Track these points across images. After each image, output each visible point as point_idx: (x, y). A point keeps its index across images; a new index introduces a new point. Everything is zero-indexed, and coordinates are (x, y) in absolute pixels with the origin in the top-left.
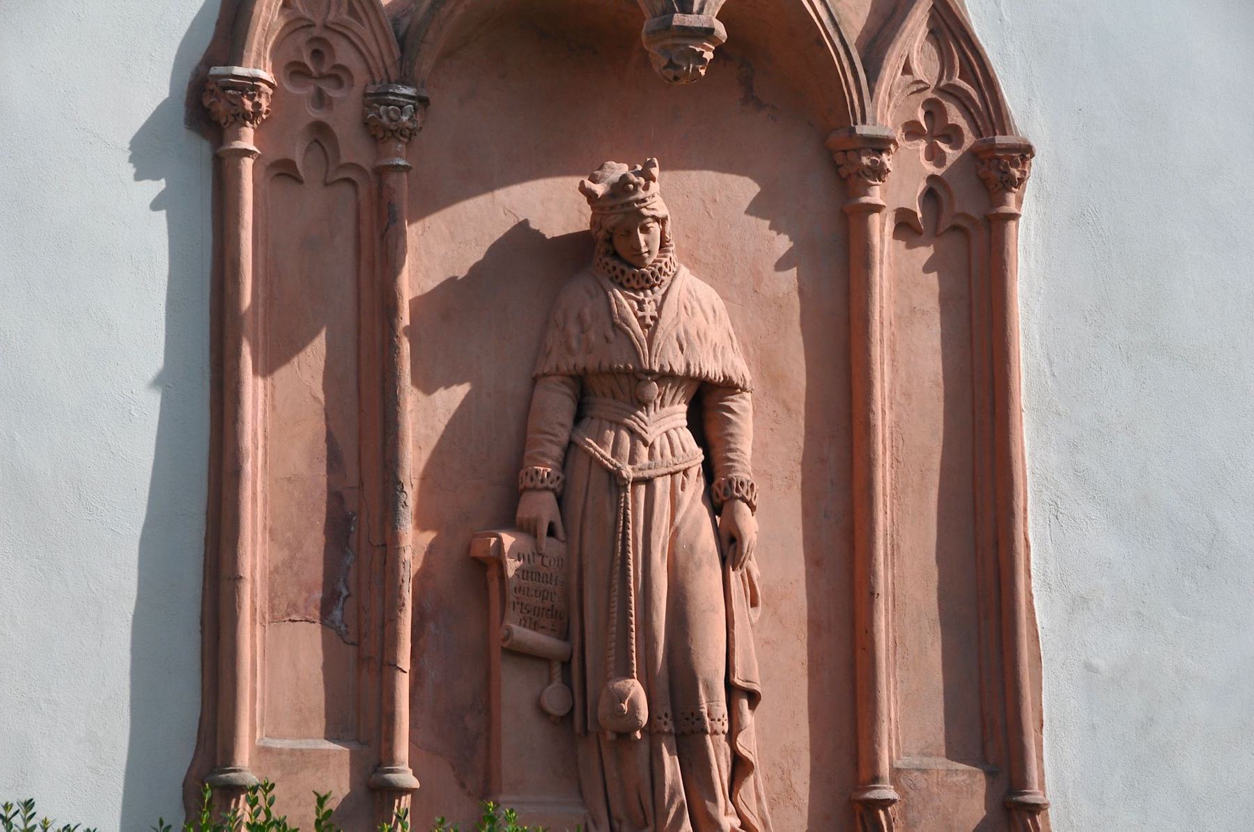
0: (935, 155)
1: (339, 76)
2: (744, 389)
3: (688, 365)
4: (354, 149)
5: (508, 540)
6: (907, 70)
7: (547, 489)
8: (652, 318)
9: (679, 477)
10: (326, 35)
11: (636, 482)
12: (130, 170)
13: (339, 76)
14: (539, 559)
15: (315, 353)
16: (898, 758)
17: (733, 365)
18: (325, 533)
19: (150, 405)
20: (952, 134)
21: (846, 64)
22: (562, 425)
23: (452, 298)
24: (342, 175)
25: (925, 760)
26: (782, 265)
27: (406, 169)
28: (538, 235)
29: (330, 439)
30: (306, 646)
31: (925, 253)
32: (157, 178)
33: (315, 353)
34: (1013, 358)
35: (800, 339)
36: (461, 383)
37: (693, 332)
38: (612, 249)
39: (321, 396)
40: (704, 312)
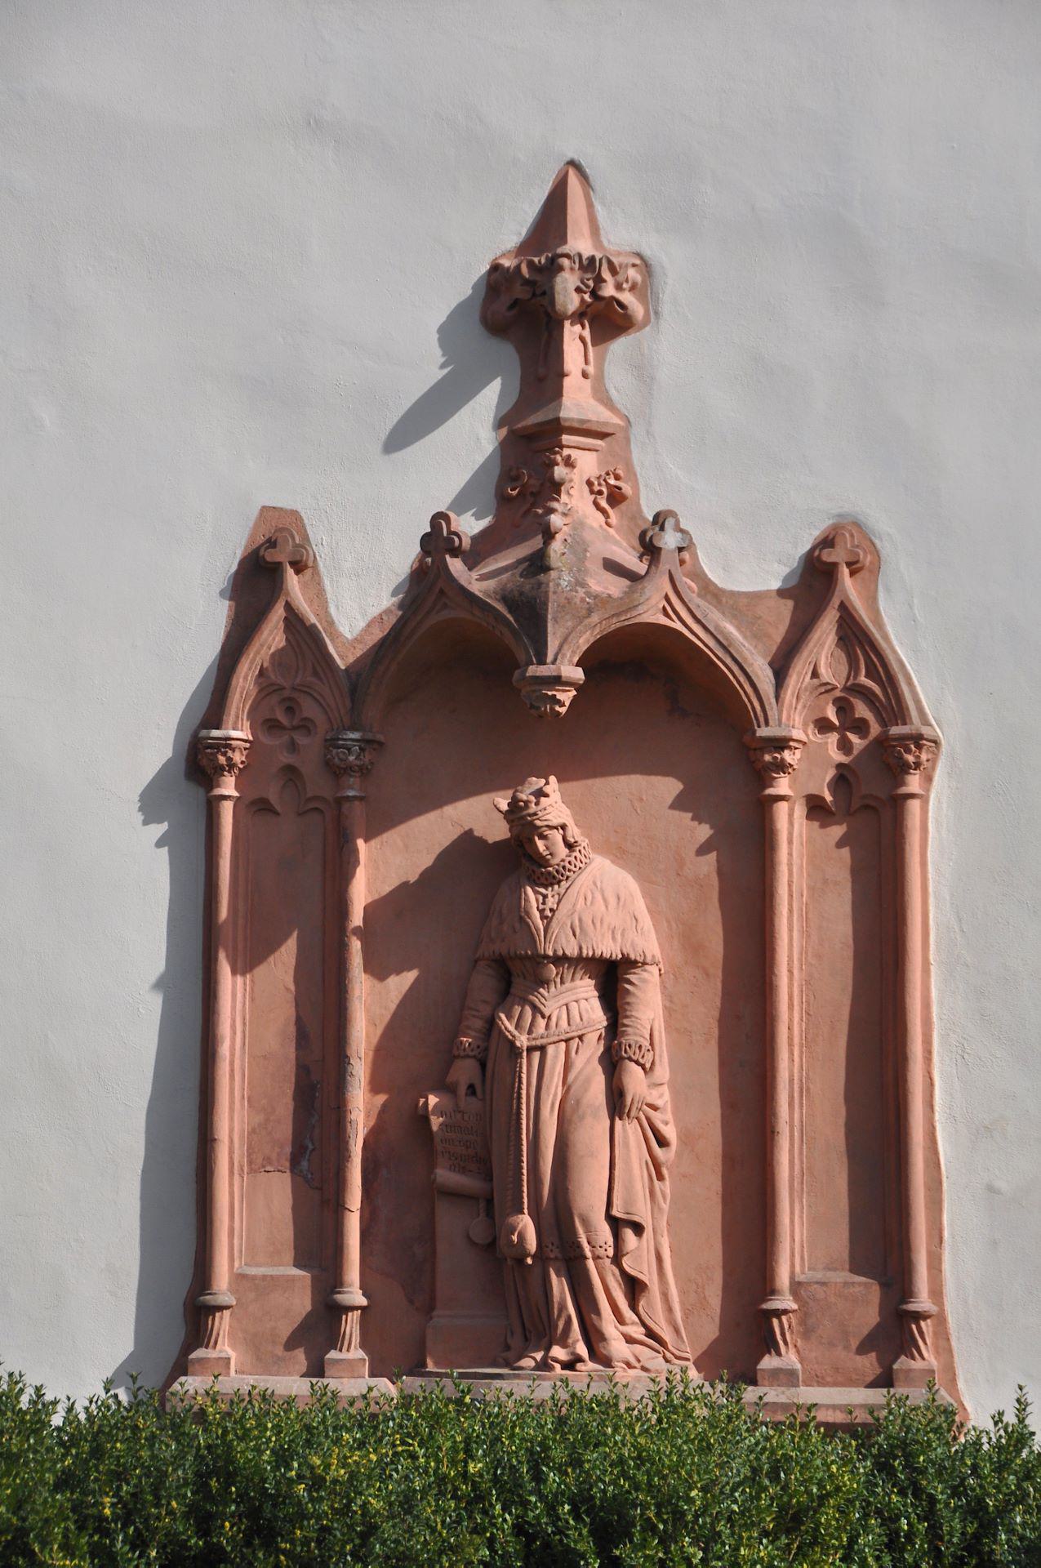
0: (844, 746)
1: (306, 726)
2: (644, 963)
3: (581, 948)
4: (317, 784)
5: (433, 1100)
6: (815, 674)
7: (468, 1056)
8: (551, 910)
9: (574, 1043)
10: (295, 695)
11: (530, 1049)
12: (140, 817)
13: (306, 726)
14: (459, 1116)
15: (288, 952)
16: (803, 1273)
17: (633, 944)
18: (294, 1099)
19: (153, 1005)
20: (861, 727)
21: (742, 679)
22: (485, 1002)
23: (399, 904)
24: (311, 805)
25: (830, 1274)
26: (702, 850)
27: (361, 799)
28: (481, 841)
29: (299, 1022)
30: (280, 1189)
31: (838, 831)
32: (160, 821)
33: (288, 952)
34: (909, 922)
35: (719, 913)
36: (410, 970)
37: (587, 921)
38: (521, 858)
39: (293, 988)
40: (605, 900)
